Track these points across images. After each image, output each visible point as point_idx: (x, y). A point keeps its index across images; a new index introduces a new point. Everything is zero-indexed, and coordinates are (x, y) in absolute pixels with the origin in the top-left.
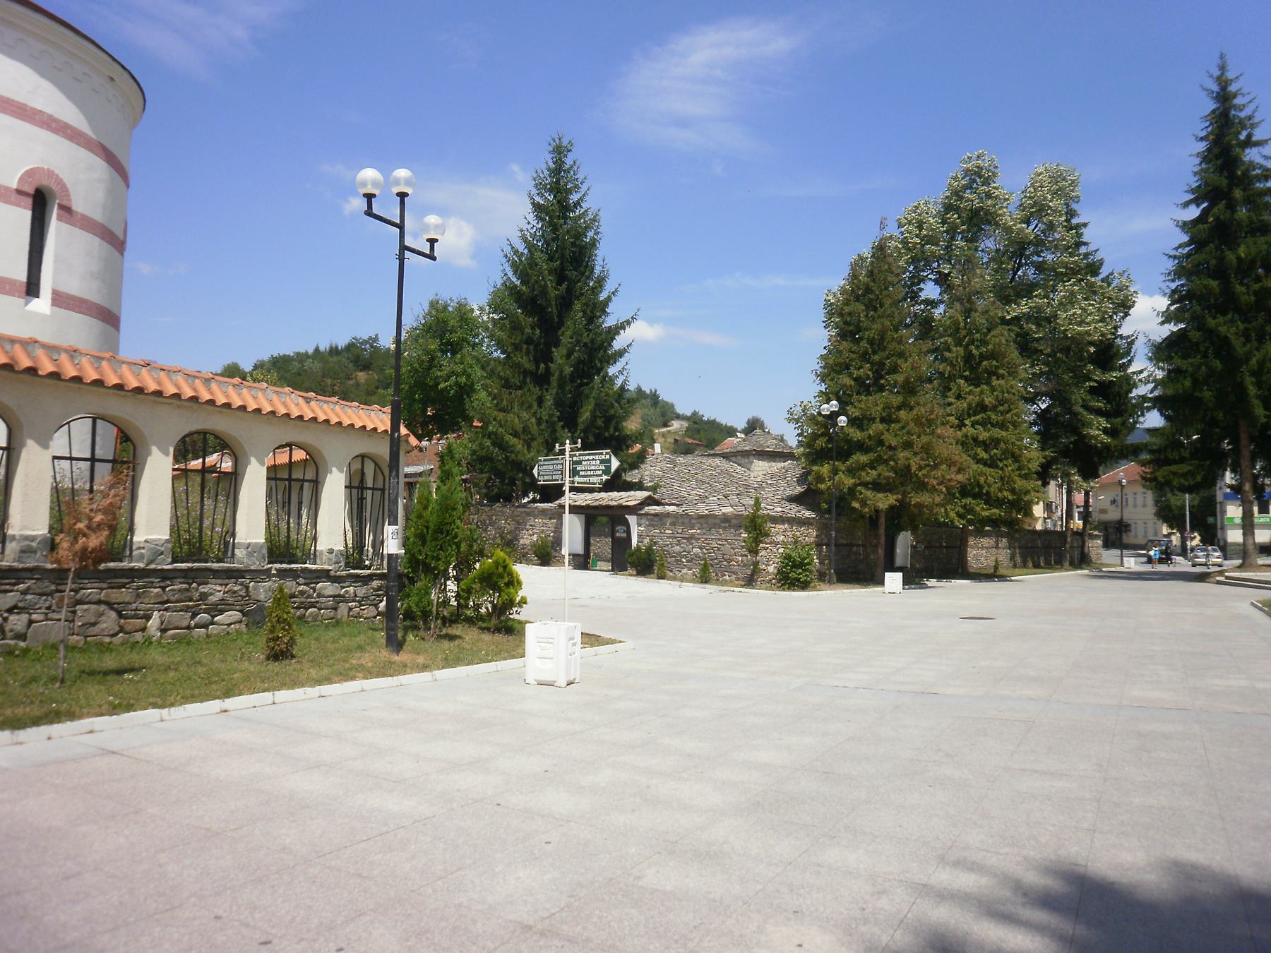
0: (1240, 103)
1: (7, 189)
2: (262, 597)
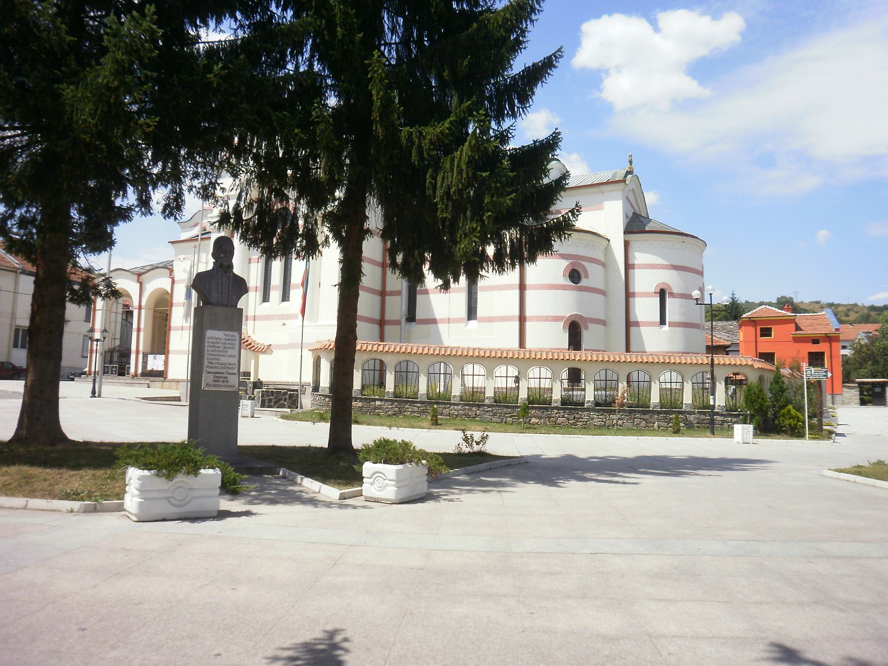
0: (118, 199)
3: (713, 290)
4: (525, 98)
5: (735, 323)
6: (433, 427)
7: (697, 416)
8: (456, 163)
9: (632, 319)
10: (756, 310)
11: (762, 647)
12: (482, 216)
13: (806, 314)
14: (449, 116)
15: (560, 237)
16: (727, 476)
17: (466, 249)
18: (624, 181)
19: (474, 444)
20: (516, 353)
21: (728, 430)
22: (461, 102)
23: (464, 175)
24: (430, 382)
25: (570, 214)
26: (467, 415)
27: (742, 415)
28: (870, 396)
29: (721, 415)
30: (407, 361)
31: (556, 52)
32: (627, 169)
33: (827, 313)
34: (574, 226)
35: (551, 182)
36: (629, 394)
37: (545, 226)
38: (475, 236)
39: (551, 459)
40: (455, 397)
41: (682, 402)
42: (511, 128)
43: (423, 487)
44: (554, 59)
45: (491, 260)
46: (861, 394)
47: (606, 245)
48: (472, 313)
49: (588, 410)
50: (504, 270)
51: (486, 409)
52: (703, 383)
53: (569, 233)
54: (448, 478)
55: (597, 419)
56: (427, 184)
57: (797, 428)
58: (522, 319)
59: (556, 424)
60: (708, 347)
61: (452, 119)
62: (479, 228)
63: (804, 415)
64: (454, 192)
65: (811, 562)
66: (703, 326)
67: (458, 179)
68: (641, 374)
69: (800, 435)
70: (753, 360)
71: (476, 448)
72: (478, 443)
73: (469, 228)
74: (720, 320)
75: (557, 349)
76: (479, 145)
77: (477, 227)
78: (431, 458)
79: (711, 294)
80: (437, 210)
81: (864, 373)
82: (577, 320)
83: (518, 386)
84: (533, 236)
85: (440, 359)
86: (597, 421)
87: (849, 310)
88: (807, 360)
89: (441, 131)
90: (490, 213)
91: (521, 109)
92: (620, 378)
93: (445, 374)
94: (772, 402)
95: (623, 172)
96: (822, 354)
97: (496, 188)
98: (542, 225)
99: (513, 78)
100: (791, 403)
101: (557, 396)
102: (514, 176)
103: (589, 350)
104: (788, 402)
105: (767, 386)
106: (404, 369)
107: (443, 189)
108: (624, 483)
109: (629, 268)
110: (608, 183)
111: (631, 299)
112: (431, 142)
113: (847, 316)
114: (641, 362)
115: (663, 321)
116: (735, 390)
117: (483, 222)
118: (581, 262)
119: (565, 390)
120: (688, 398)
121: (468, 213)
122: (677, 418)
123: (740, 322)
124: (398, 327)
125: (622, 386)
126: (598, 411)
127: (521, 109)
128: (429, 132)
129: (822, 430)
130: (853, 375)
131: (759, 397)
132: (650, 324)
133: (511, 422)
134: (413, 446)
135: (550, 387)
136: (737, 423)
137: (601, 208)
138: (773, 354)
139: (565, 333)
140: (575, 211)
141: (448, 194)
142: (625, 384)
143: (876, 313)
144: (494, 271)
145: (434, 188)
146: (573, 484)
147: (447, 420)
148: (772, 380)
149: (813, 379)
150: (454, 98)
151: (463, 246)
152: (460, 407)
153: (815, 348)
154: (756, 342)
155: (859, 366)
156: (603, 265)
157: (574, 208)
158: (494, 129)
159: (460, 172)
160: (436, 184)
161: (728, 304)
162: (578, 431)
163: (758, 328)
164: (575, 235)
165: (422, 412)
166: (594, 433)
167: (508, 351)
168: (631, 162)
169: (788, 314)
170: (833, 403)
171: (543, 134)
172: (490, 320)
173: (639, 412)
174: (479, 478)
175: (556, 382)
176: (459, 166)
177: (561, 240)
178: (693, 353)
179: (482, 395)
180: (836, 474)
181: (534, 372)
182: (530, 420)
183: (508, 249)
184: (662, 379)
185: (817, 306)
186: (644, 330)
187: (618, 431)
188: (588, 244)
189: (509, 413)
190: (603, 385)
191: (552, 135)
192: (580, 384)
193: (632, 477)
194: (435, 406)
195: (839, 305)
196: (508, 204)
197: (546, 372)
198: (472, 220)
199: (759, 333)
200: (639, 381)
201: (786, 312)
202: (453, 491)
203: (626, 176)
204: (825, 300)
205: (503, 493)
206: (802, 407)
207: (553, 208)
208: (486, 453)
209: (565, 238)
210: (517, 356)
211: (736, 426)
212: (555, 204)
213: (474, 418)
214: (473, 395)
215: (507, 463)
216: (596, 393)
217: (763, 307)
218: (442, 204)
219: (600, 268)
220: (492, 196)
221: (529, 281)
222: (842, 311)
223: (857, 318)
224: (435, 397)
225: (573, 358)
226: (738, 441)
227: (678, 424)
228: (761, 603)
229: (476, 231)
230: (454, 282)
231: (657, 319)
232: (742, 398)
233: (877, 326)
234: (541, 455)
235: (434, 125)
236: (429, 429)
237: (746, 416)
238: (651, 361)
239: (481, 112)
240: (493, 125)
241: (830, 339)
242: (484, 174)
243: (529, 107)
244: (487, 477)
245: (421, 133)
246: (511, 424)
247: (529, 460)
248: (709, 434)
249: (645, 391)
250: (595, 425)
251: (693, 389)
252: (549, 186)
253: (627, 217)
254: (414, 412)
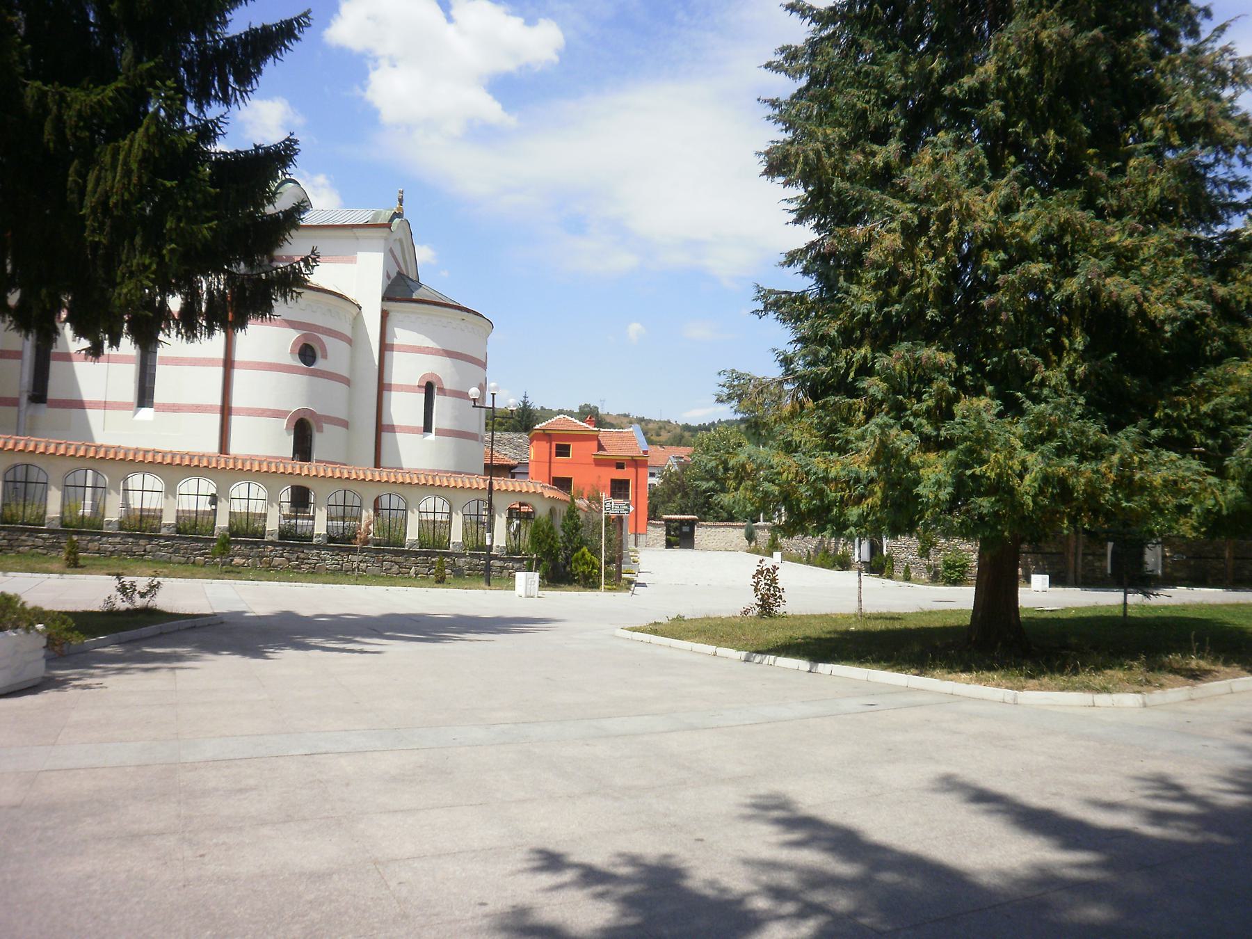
1: (414, 386)
2: (461, 565)
3: (497, 388)
4: (246, 77)
5: (525, 435)
6: (68, 570)
7: (468, 560)
8: (121, 157)
9: (385, 421)
10: (553, 420)
11: (519, 856)
12: (160, 248)
13: (612, 430)
14: (115, 79)
15: (284, 295)
16: (502, 641)
17: (131, 295)
18: (388, 226)
19: (137, 597)
20: (214, 460)
21: (509, 580)
22: (138, 60)
23: (135, 180)
24: (66, 499)
25: (302, 264)
26: (133, 554)
27: (527, 559)
28: (677, 536)
29: (501, 559)
30: (27, 465)
31: (300, 17)
32: (395, 210)
33: (635, 431)
34: (306, 281)
35: (278, 213)
36: (376, 527)
37: (263, 276)
38: (147, 277)
39: (259, 617)
40: (110, 522)
41: (449, 539)
42: (221, 119)
43: (38, 669)
44: (296, 25)
45: (174, 319)
46: (668, 533)
47: (355, 314)
48: (145, 396)
49: (317, 547)
50: (195, 336)
51: (163, 542)
52: (478, 515)
53: (298, 290)
54: (86, 652)
55: (330, 561)
56: (69, 183)
57: (592, 577)
58: (226, 411)
59: (270, 566)
60: (486, 466)
61: (120, 85)
62: (154, 267)
63: (600, 560)
64: (116, 205)
65: (587, 745)
66: (482, 438)
67: (124, 184)
68: (395, 499)
69: (595, 586)
70: (543, 486)
71: (139, 602)
72: (143, 595)
73: (138, 265)
74: (506, 430)
75: (277, 458)
76: (161, 135)
77: (151, 264)
78: (54, 621)
79: (493, 394)
80: (84, 228)
81: (671, 508)
82: (307, 417)
83: (215, 510)
84: (245, 289)
85: (87, 465)
86: (330, 563)
87: (660, 428)
88: (608, 489)
89: (99, 100)
90: (173, 246)
91: (238, 93)
92: (365, 503)
93: (94, 487)
94: (564, 543)
95: (389, 214)
96: (627, 481)
97: (186, 208)
98: (259, 274)
99: (229, 41)
100: (587, 545)
101: (273, 525)
102: (217, 193)
103: (322, 462)
104: (583, 543)
105: (559, 521)
106: (20, 476)
107: (97, 196)
108: (362, 652)
109: (385, 350)
110: (366, 226)
111: (385, 393)
112: (80, 115)
113: (659, 435)
114: (395, 482)
115: (427, 427)
116: (519, 526)
117: (162, 257)
118: (320, 336)
119: (285, 517)
120: (456, 536)
121: (138, 240)
122: (441, 562)
123: (532, 434)
124: (12, 411)
125: (367, 514)
126: (332, 549)
127: (238, 93)
128: (76, 97)
129: (620, 578)
130: (661, 509)
131: (548, 537)
132: (410, 430)
133: (202, 562)
134: (21, 602)
135: (263, 512)
136: (519, 570)
137: (353, 261)
138: (569, 480)
139: (289, 435)
140: (311, 260)
141: (104, 203)
142: (372, 512)
143: (690, 433)
144: (180, 336)
145: (82, 192)
146: (289, 654)
147: (95, 559)
148: (565, 514)
149: (613, 513)
150: (127, 50)
151: (125, 291)
152: (118, 539)
153: (619, 475)
154: (550, 462)
155: (667, 499)
156: (349, 341)
157: (309, 256)
158: (191, 116)
159: (128, 173)
160: (85, 186)
161: (515, 409)
162: (302, 577)
163: (554, 444)
164: (307, 294)
165: (49, 546)
166: (325, 580)
167: (201, 457)
168: (401, 201)
169: (591, 428)
170: (636, 545)
171: (272, 137)
172: (175, 408)
173: (390, 552)
174: (138, 648)
175: (272, 506)
176: (126, 163)
177: (286, 300)
178: (466, 474)
179: (156, 522)
180: (629, 634)
181: (239, 489)
182: (232, 560)
183: (203, 304)
184: (422, 507)
185: (625, 420)
186: (400, 436)
187: (359, 578)
188: (330, 310)
189: (200, 550)
190: (340, 513)
191: (284, 142)
192: (308, 510)
193: (375, 644)
194: (75, 538)
195: (650, 421)
196: (204, 237)
197: (258, 491)
198: (142, 253)
199: (554, 450)
200: (390, 509)
201: (588, 426)
202: (92, 671)
203: (391, 220)
204: (635, 413)
205: (178, 672)
206: (597, 549)
207: (278, 253)
208: (155, 610)
209: (292, 297)
210: (214, 465)
211: (518, 574)
212: (280, 246)
213: (143, 555)
214: (141, 520)
215: (189, 625)
216: (330, 523)
217: (562, 416)
218: (94, 220)
219: (344, 345)
220: (179, 220)
221: (239, 355)
222: (652, 429)
223: (669, 439)
224: (74, 523)
225: (298, 472)
226: (520, 594)
227: (442, 571)
228: (524, 801)
229: (150, 271)
230: (111, 346)
231: (421, 423)
232: (528, 536)
233: (690, 450)
234: (245, 612)
235: (88, 89)
236: (62, 573)
237: (531, 560)
238: (408, 481)
239: (169, 83)
240: (191, 107)
241: (637, 463)
242: (168, 184)
243: (251, 91)
244: (156, 647)
245: (62, 97)
246: (203, 566)
247: (225, 620)
248: (483, 584)
249: (398, 524)
250: (327, 569)
251: (464, 523)
252: (274, 218)
253: (388, 277)
254: (37, 547)
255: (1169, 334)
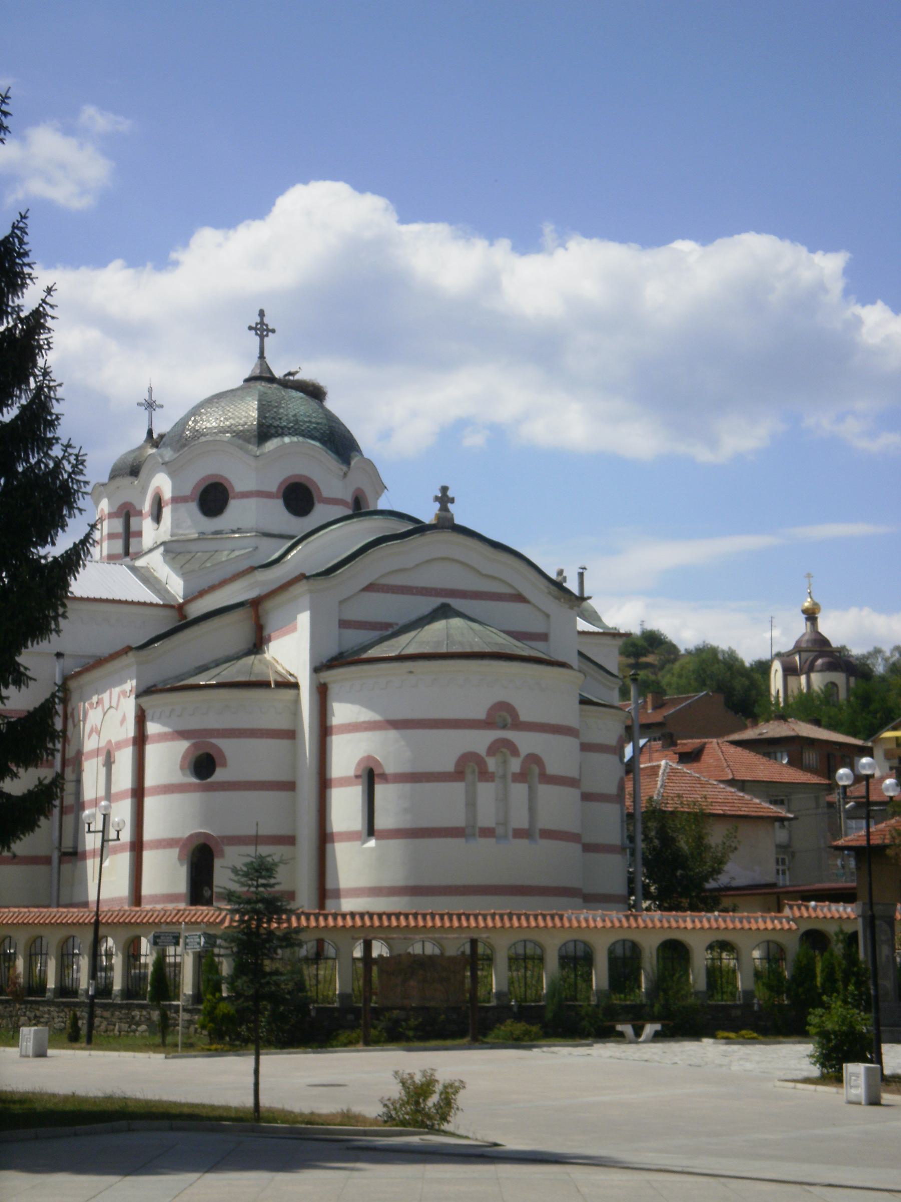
115: (371, 831)
126: (58, 1005)
132: (350, 836)
255: (38, 615)
